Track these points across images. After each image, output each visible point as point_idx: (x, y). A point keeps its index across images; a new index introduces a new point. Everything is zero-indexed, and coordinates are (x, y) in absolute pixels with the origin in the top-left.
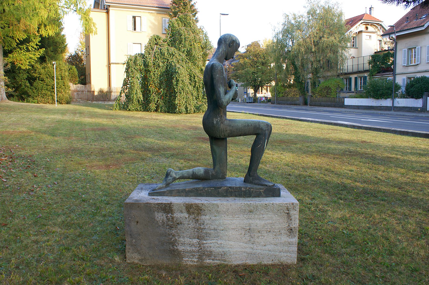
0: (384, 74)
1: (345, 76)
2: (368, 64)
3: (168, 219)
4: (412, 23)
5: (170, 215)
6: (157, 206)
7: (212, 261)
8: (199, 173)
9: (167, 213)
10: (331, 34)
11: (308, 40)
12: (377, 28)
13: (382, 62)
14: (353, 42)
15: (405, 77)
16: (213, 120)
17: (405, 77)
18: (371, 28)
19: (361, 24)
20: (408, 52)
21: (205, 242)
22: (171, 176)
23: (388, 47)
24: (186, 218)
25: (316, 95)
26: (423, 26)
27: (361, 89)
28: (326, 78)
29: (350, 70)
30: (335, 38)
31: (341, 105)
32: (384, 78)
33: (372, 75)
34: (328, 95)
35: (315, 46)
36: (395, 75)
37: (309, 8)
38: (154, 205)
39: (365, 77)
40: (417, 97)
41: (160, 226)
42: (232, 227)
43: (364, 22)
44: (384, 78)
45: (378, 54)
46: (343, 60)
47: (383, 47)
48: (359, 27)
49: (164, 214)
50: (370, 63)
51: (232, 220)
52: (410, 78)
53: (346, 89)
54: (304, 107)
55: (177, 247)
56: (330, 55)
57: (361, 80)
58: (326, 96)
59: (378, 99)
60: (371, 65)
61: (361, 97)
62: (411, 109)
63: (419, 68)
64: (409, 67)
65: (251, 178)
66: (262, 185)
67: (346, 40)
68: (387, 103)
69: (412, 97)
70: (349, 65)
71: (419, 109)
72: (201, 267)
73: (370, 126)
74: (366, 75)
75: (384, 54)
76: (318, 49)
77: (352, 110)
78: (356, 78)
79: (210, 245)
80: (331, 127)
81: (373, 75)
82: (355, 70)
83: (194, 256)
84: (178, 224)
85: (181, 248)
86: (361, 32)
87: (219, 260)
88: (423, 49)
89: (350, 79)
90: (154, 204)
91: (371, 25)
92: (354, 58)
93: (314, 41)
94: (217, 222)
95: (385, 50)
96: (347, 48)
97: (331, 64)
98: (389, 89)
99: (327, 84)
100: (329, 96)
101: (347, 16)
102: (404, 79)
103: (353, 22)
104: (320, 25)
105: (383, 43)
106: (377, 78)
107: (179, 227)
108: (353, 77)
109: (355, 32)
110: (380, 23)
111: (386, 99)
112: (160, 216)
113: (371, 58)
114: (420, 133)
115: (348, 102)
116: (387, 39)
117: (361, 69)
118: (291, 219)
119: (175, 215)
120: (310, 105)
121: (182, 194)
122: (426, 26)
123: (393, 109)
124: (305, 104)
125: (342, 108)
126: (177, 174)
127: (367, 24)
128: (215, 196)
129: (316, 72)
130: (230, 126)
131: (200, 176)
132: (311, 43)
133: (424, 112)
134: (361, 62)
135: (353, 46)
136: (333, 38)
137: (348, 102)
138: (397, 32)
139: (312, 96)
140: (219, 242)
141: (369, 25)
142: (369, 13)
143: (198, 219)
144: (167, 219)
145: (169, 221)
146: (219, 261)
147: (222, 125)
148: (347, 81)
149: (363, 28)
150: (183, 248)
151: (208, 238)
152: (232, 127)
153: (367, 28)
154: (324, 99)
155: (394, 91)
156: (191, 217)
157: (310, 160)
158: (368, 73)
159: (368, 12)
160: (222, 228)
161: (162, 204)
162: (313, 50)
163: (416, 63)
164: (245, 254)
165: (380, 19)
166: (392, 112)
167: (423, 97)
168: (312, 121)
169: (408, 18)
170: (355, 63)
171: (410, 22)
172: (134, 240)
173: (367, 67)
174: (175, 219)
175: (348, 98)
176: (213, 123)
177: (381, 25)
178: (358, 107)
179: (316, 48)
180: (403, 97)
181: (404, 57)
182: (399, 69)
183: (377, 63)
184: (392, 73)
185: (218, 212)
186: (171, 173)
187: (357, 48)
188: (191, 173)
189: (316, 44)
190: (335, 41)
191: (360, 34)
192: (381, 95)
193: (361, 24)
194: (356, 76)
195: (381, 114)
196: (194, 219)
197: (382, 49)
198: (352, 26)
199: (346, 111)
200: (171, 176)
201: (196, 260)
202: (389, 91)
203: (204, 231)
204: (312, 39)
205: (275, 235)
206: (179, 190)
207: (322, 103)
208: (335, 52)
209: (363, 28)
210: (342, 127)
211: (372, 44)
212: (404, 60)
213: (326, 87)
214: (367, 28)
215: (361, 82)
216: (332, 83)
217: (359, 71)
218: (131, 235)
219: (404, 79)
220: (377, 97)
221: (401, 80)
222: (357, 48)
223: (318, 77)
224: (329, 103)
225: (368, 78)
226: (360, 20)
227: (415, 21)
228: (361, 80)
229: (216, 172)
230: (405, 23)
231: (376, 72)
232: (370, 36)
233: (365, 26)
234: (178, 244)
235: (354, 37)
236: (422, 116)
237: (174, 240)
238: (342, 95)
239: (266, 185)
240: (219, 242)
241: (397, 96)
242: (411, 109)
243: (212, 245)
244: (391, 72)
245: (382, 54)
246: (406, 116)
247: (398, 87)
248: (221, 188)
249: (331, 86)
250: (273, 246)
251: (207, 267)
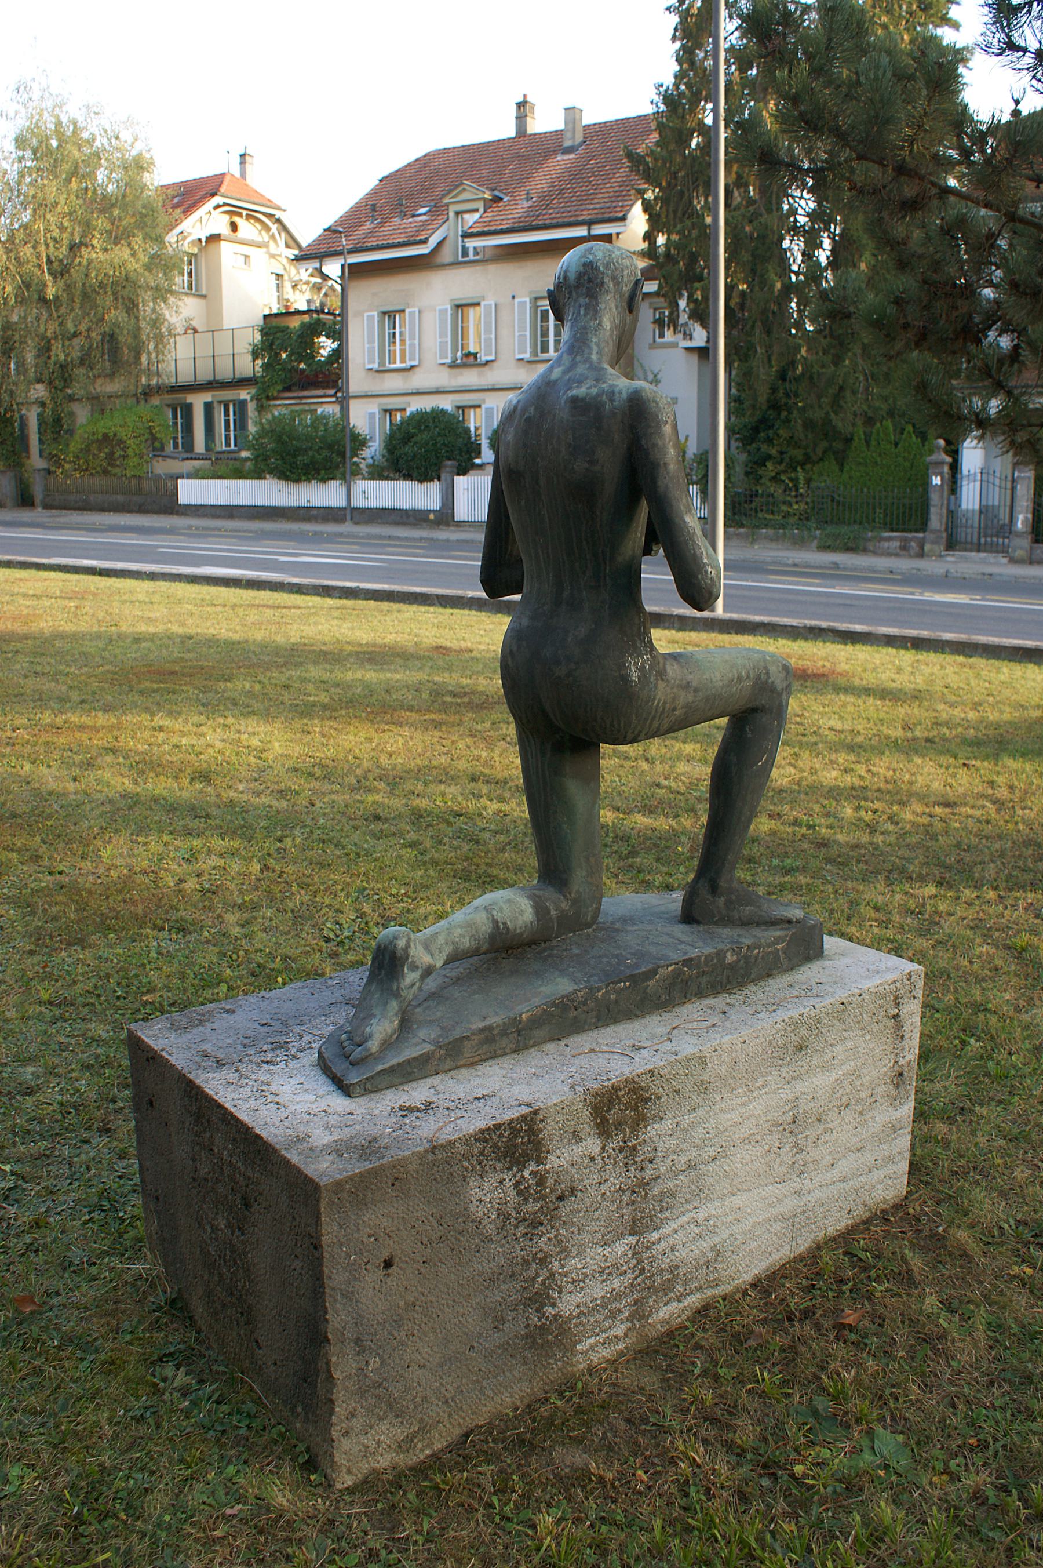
0: (306, 393)
1: (168, 398)
2: (250, 358)
3: (523, 1194)
4: (387, 227)
5: (532, 1166)
6: (477, 1148)
7: (675, 1304)
8: (520, 923)
9: (518, 1163)
10: (117, 237)
11: (27, 251)
12: (268, 229)
13: (296, 354)
14: (190, 274)
15: (373, 407)
16: (621, 666)
17: (373, 407)
18: (247, 229)
19: (216, 208)
20: (381, 323)
21: (655, 1236)
22: (414, 967)
23: (309, 302)
24: (593, 1159)
25: (67, 466)
26: (425, 241)
27: (228, 444)
28: (99, 404)
29: (185, 376)
30: (134, 255)
31: (170, 506)
32: (307, 407)
33: (263, 400)
34: (113, 466)
35: (55, 278)
36: (344, 403)
37: (21, 123)
38: (462, 1149)
39: (242, 405)
40: (424, 477)
41: (488, 1239)
42: (744, 1131)
43: (225, 204)
44: (307, 407)
45: (275, 322)
46: (159, 338)
47: (288, 300)
48: (204, 221)
49: (507, 1175)
50: (255, 354)
51: (743, 1104)
52: (389, 411)
53: (176, 446)
54: (25, 515)
55: (554, 1305)
56: (116, 315)
57: (227, 414)
58: (105, 472)
59: (297, 481)
60: (259, 362)
61: (239, 474)
62: (408, 517)
63: (419, 380)
64: (387, 375)
65: (721, 901)
66: (773, 923)
67: (163, 263)
68: (327, 494)
69: (408, 477)
70: (180, 359)
71: (432, 517)
72: (660, 1350)
73: (386, 587)
74: (244, 394)
75: (303, 325)
76: (68, 287)
77: (295, 526)
78: (208, 407)
79: (671, 1241)
80: (265, 596)
81: (268, 398)
82: (205, 375)
83: (613, 1314)
84: (561, 1198)
85: (567, 1304)
86: (214, 239)
87: (700, 1289)
88: (425, 315)
89: (188, 409)
90: (466, 1141)
91: (248, 217)
92: (195, 331)
93: (49, 261)
94: (699, 1133)
95: (298, 312)
96: (172, 292)
97: (117, 351)
98: (330, 447)
99: (106, 425)
100: (117, 470)
101: (168, 171)
102: (372, 415)
103: (191, 195)
104: (73, 197)
105: (288, 286)
106: (281, 408)
107: (565, 1209)
108: (198, 402)
109: (194, 237)
110: (278, 214)
111: (324, 480)
112: (489, 1192)
113: (258, 337)
114: (376, 591)
115: (191, 491)
116: (304, 272)
117: (225, 372)
118: (902, 1037)
119: (553, 1162)
120: (46, 507)
121: (504, 1042)
122: (433, 241)
123: (348, 517)
124: (25, 500)
125: (172, 513)
126: (433, 948)
127: (234, 212)
128: (629, 1015)
129: (59, 378)
130: (687, 686)
131: (521, 934)
132: (39, 266)
133: (448, 525)
134: (224, 348)
135: (190, 287)
136: (126, 253)
137: (191, 491)
138: (351, 252)
139: (49, 472)
140: (701, 1216)
141: (240, 215)
142: (238, 175)
143: (634, 1148)
144: (519, 1193)
145: (526, 1199)
146: (699, 1295)
147: (661, 685)
148: (175, 417)
149: (219, 224)
150: (578, 1298)
151: (667, 1214)
152: (696, 690)
153: (234, 227)
154: (98, 482)
155: (348, 455)
156: (610, 1146)
157: (354, 742)
158: (253, 391)
159: (236, 171)
160: (712, 1152)
161: (497, 1127)
162: (51, 292)
163: (409, 363)
164: (777, 1227)
165: (277, 201)
166: (347, 527)
167: (443, 476)
168: (153, 576)
169: (374, 208)
170: (204, 351)
171: (382, 224)
172: (374, 1362)
173: (247, 366)
174: (550, 1182)
175: (189, 476)
176: (625, 679)
177: (278, 221)
178: (230, 512)
179: (61, 283)
180: (377, 473)
181: (371, 341)
182: (357, 380)
183: (277, 355)
184: (332, 392)
185: (703, 1088)
186: (412, 952)
187: (204, 297)
188: (485, 928)
189: (60, 270)
190: (133, 265)
191: (212, 246)
192: (306, 466)
193: (216, 208)
194: (208, 397)
195: (316, 533)
196: (621, 1150)
197: (287, 307)
198: (187, 211)
199: (190, 527)
200: (414, 967)
201: (620, 1330)
202: (321, 455)
203: (656, 1191)
204: (43, 248)
205: (861, 1113)
206: (489, 1028)
207: (92, 498)
208: (132, 307)
209: (219, 224)
210: (114, 579)
211: (254, 284)
212: (371, 350)
213: (105, 436)
214: (234, 227)
215: (227, 422)
216: (126, 423)
217: (217, 382)
218: (358, 1341)
219: (372, 415)
220: (294, 476)
221: (363, 417)
222: (204, 297)
223: (71, 399)
224: (120, 498)
225: (251, 407)
226: (213, 195)
227: (397, 221)
228: (227, 414)
229: (575, 902)
230: (368, 226)
231: (280, 388)
232: (247, 257)
233: (227, 217)
234: (560, 1292)
235: (191, 255)
236: (448, 540)
237: (543, 1282)
238: (162, 467)
239: (789, 922)
240: (701, 1216)
241: (356, 473)
242: (408, 517)
243: (680, 1237)
244: (328, 387)
245: (295, 323)
246: (399, 538)
247: (359, 442)
248: (655, 972)
249: (122, 434)
250: (852, 1157)
251: (672, 1334)
